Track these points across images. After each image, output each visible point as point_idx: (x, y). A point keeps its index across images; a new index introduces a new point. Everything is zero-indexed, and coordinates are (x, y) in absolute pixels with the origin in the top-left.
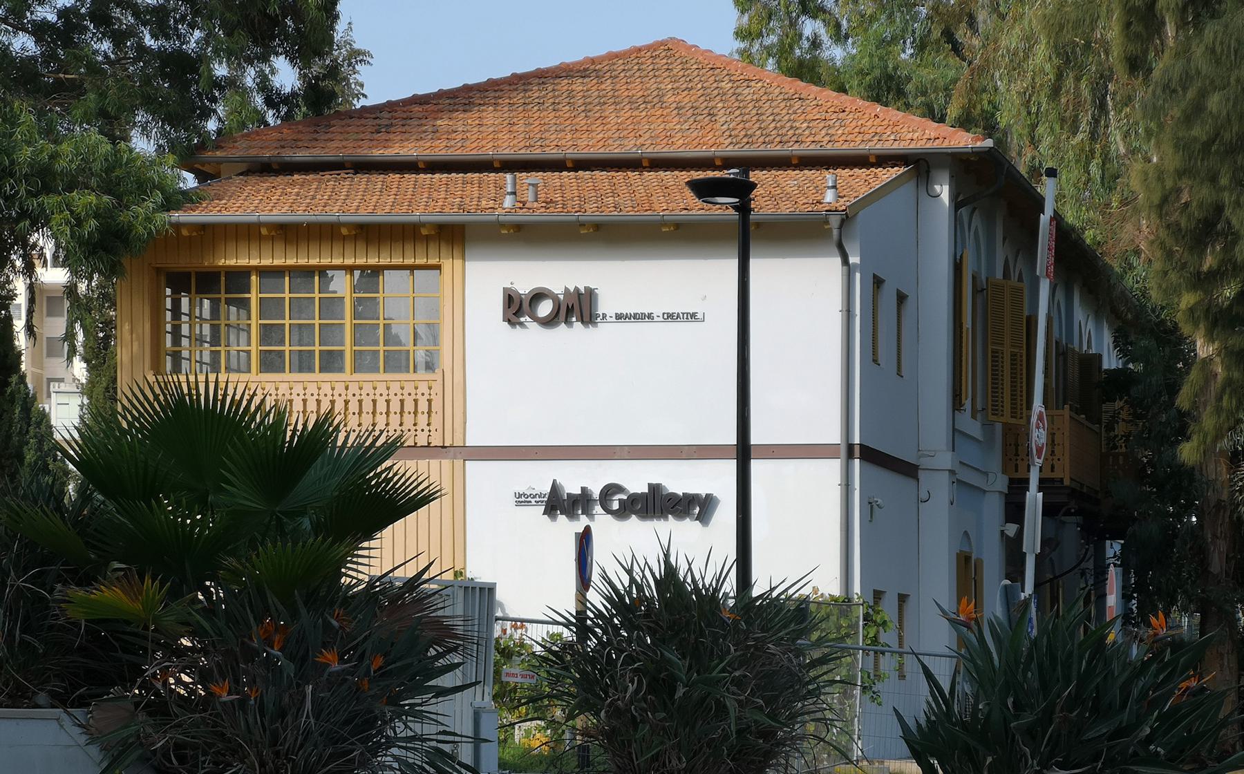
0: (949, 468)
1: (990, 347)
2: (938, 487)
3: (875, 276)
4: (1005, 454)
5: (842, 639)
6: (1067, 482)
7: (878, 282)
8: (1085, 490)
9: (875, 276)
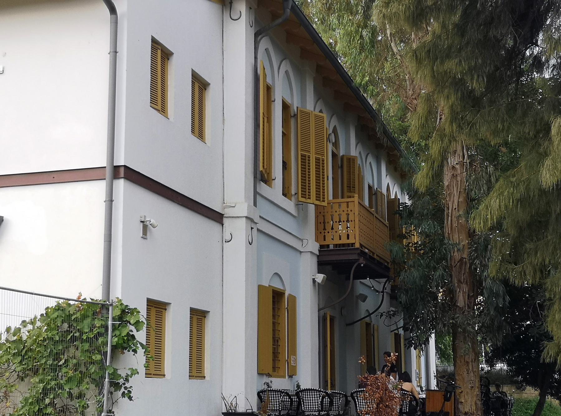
0: (246, 215)
1: (300, 153)
2: (237, 229)
3: (155, 42)
4: (317, 228)
5: (96, 337)
6: (357, 245)
7: (161, 54)
8: (375, 257)
9: (155, 42)
